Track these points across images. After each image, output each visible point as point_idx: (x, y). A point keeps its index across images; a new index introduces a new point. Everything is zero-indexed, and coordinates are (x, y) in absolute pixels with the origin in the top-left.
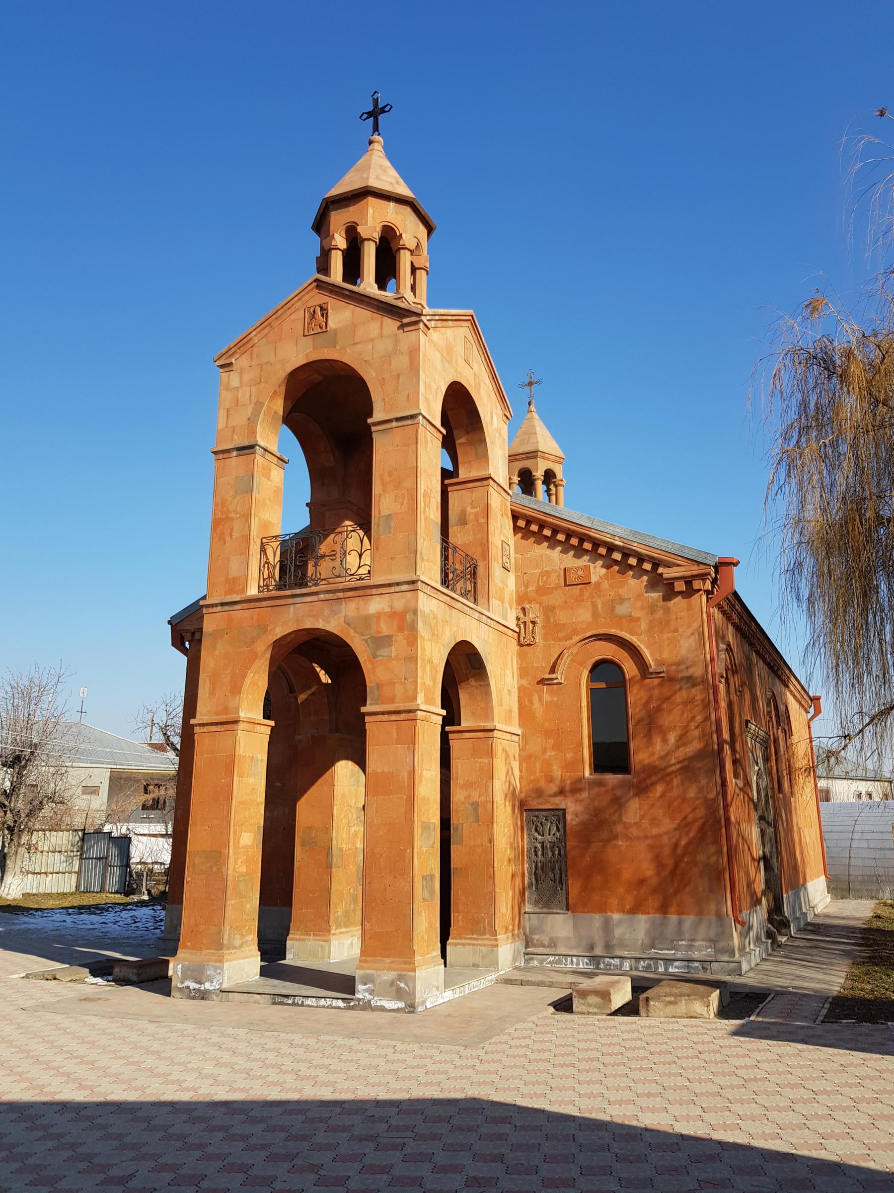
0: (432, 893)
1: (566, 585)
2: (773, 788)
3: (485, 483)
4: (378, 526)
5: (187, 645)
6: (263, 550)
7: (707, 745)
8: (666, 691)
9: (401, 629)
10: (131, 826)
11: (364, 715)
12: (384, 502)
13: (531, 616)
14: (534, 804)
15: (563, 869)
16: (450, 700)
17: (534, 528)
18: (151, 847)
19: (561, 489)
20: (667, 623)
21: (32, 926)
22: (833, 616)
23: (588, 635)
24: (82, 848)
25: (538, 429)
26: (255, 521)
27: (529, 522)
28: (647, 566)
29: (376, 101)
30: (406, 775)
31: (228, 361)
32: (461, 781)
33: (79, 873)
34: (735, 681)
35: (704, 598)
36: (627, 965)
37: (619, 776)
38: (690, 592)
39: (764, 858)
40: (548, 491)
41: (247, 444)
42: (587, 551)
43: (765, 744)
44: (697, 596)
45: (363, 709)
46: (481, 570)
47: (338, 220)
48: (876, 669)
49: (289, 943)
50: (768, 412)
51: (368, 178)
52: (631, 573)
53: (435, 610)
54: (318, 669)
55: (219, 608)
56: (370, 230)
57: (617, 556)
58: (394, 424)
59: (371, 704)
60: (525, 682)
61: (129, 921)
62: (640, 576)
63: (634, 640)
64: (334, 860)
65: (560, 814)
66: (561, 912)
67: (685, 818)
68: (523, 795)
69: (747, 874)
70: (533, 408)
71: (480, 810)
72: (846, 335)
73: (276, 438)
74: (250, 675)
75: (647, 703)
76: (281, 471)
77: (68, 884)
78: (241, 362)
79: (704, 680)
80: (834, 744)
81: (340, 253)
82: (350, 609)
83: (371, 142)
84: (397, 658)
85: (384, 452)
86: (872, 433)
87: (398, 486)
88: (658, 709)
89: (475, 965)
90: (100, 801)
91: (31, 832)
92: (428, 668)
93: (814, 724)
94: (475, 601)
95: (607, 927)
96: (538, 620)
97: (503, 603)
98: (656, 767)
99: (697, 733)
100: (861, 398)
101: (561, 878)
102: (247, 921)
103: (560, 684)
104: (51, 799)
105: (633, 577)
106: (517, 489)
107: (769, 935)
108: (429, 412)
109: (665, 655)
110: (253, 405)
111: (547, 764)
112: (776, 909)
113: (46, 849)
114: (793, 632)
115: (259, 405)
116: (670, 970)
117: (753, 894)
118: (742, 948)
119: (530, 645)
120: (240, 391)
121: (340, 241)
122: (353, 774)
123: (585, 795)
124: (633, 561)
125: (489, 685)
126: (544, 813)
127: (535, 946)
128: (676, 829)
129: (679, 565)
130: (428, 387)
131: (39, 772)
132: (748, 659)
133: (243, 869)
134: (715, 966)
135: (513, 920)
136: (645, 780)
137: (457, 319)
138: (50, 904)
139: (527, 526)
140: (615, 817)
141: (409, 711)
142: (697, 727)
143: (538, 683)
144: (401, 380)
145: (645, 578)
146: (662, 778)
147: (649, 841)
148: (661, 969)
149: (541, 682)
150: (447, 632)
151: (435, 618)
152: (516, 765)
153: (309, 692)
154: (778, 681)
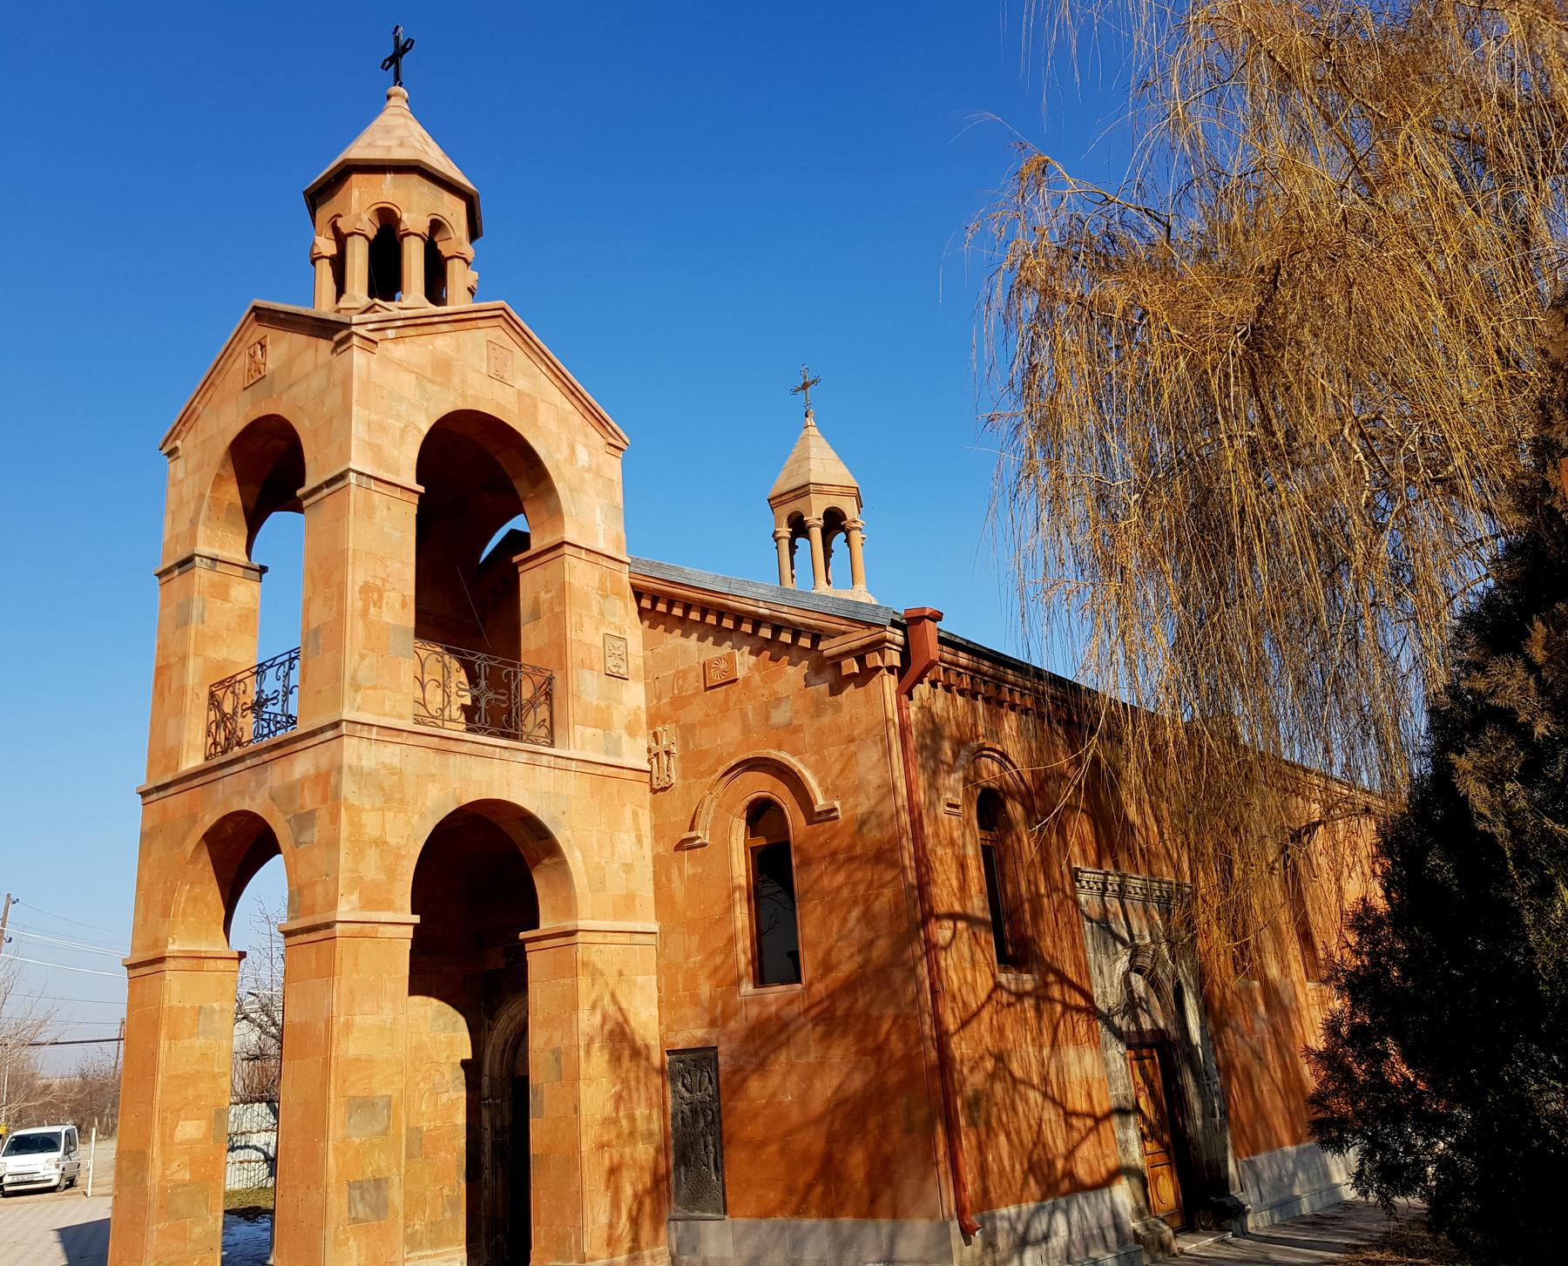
1: (707, 689)
19: (856, 536)
23: (733, 763)
30: (322, 1025)
32: (540, 1017)
38: (865, 675)
46: (558, 685)
58: (326, 491)
66: (715, 1215)
70: (810, 421)
71: (563, 1059)
96: (674, 749)
102: (195, 1252)
103: (704, 845)
108: (379, 466)
119: (664, 789)
129: (844, 633)
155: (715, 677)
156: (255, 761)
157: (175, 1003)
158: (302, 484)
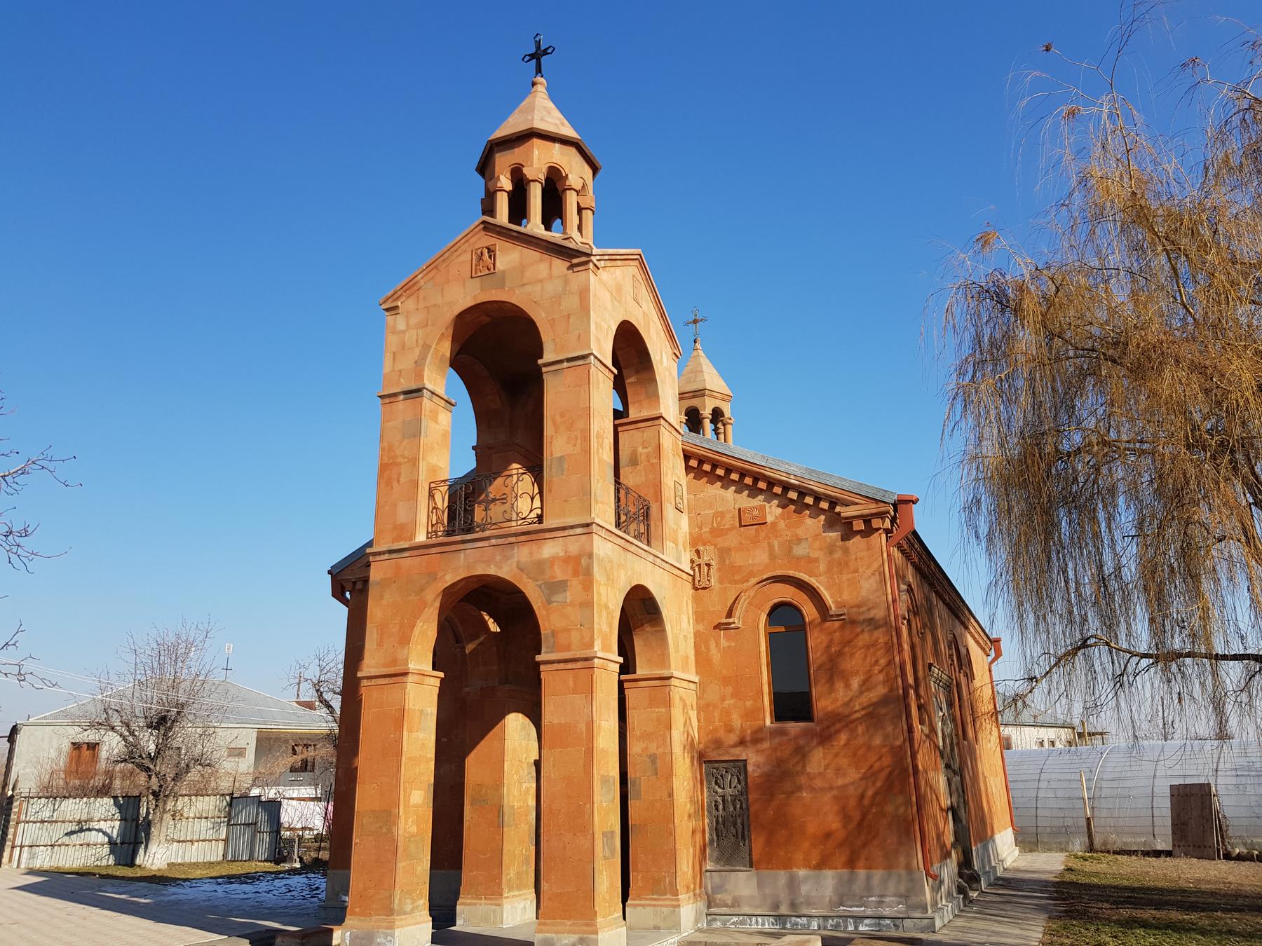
0: (613, 851)
1: (741, 526)
2: (957, 735)
3: (656, 422)
5: (348, 595)
6: (431, 496)
7: (891, 690)
8: (847, 634)
9: (576, 573)
10: (281, 789)
11: (538, 664)
12: (556, 444)
13: (706, 558)
14: (714, 755)
15: (745, 824)
16: (625, 648)
17: (707, 467)
18: (305, 812)
19: (729, 427)
20: (847, 564)
21: (181, 897)
22: (1015, 555)
24: (229, 814)
25: (704, 367)
26: (423, 466)
27: (701, 462)
28: (824, 505)
29: (538, 44)
30: (583, 726)
31: (394, 304)
32: (638, 733)
33: (226, 840)
34: (917, 623)
35: (884, 536)
36: (814, 925)
37: (801, 724)
38: (869, 531)
39: (952, 808)
40: (716, 430)
41: (414, 387)
42: (761, 490)
43: (948, 688)
44: (876, 535)
45: (538, 658)
47: (504, 162)
48: (1060, 606)
49: (459, 908)
50: (943, 347)
51: (532, 120)
52: (807, 512)
53: (610, 553)
54: (487, 617)
55: (387, 556)
56: (536, 170)
57: (793, 495)
58: (566, 365)
60: (701, 627)
61: (283, 889)
62: (818, 515)
63: (813, 581)
64: (506, 818)
65: (740, 766)
67: (871, 767)
68: (702, 746)
69: (937, 825)
70: (698, 345)
71: (658, 761)
72: (1020, 268)
73: (442, 381)
74: (419, 624)
75: (828, 647)
76: (449, 414)
77: (214, 852)
78: (406, 304)
79: (886, 623)
80: (1022, 687)
81: (505, 195)
82: (523, 554)
83: (534, 84)
84: (572, 604)
85: (555, 393)
86: (1048, 367)
87: (570, 427)
88: (840, 653)
89: (657, 928)
90: (246, 764)
91: (176, 797)
92: (604, 613)
93: (994, 666)
94: (649, 544)
95: (793, 884)
97: (677, 545)
98: (839, 714)
99: (881, 677)
100: (1037, 333)
101: (743, 833)
104: (197, 761)
105: (810, 516)
106: (684, 429)
107: (961, 890)
109: (846, 597)
111: (727, 713)
112: (965, 862)
113: (192, 815)
114: (973, 572)
115: (426, 347)
116: (861, 928)
117: (943, 846)
118: (934, 904)
119: (705, 588)
121: (506, 183)
122: (523, 728)
123: (766, 745)
124: (809, 500)
125: (664, 630)
126: (724, 765)
127: (717, 906)
128: (861, 779)
130: (598, 326)
131: (185, 734)
132: (928, 599)
133: (414, 829)
134: (907, 923)
135: (694, 878)
136: (828, 727)
137: (626, 259)
138: (198, 873)
139: (702, 466)
140: (799, 768)
141: (586, 659)
142: (880, 672)
143: (715, 628)
145: (823, 517)
146: (846, 726)
147: (834, 792)
148: (851, 928)
149: (718, 627)
150: (623, 578)
151: (611, 562)
152: (693, 715)
153: (477, 642)
154: (957, 623)
155: (747, 519)
156: (500, 541)
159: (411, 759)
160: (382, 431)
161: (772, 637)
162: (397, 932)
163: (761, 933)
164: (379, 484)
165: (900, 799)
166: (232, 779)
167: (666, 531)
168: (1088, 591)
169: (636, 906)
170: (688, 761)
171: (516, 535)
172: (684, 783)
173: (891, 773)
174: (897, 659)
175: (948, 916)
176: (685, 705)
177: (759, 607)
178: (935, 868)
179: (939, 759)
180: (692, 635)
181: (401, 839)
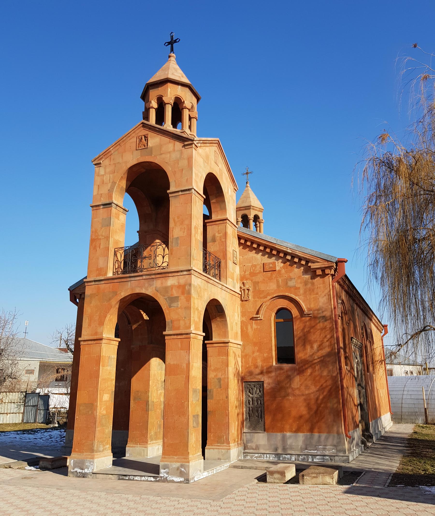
0: (198, 424)
1: (264, 271)
2: (364, 370)
3: (225, 221)
4: (172, 243)
5: (78, 300)
6: (115, 254)
7: (332, 350)
8: (313, 323)
9: (183, 293)
10: (50, 389)
12: (175, 231)
14: (249, 379)
15: (262, 411)
17: (249, 243)
18: (59, 400)
19: (262, 224)
20: (313, 290)
23: (274, 296)
24: (25, 401)
25: (251, 195)
26: (111, 240)
27: (246, 241)
28: (303, 262)
29: (172, 37)
30: (185, 365)
31: (99, 162)
33: (23, 413)
34: (346, 318)
35: (331, 278)
36: (293, 458)
38: (324, 275)
39: (361, 405)
40: (256, 225)
41: (108, 202)
42: (274, 255)
43: (361, 349)
45: (164, 333)
46: (223, 264)
47: (153, 94)
50: (360, 187)
51: (168, 74)
52: (295, 266)
54: (142, 313)
55: (93, 283)
57: (289, 257)
58: (180, 193)
59: (168, 330)
60: (244, 319)
61: (48, 437)
63: (297, 298)
64: (150, 407)
65: (261, 384)
66: (262, 432)
67: (322, 385)
68: (243, 374)
69: (352, 412)
70: (248, 185)
72: (399, 152)
73: (122, 200)
74: (108, 316)
75: (303, 329)
77: (18, 419)
78: (105, 162)
79: (331, 318)
80: (394, 349)
81: (154, 110)
82: (158, 283)
83: (169, 57)
85: (175, 207)
87: (182, 223)
88: (309, 332)
89: (219, 459)
90: (34, 377)
92: (196, 312)
94: (220, 279)
95: (284, 439)
96: (250, 289)
97: (233, 280)
98: (307, 361)
99: (327, 344)
104: (10, 376)
105: (297, 268)
107: (363, 442)
109: (312, 306)
110: (111, 184)
111: (255, 359)
112: (366, 429)
113: (7, 401)
114: (373, 294)
115: (114, 183)
116: (314, 460)
118: (350, 449)
119: (246, 301)
120: (105, 177)
121: (154, 104)
122: (159, 365)
123: (273, 374)
124: (296, 260)
125: (226, 320)
126: (253, 383)
128: (317, 391)
129: (318, 262)
132: (352, 307)
133: (105, 412)
134: (336, 458)
135: (238, 436)
136: (302, 367)
137: (211, 143)
138: (9, 429)
139: (245, 242)
140: (288, 385)
141: (187, 334)
142: (327, 341)
143: (251, 319)
144: (184, 172)
145: (302, 268)
146: (311, 366)
148: (310, 460)
149: (252, 319)
150: (206, 295)
151: (200, 288)
152: (239, 360)
154: (367, 318)
155: (267, 268)
157: (104, 354)
158: (169, 189)
159: (104, 379)
160: (92, 223)
161: (277, 325)
162: (95, 460)
163: (268, 462)
164: (90, 249)
165: (335, 401)
166: (26, 384)
167: (229, 274)
168: (427, 304)
169: (210, 449)
170: (236, 381)
171: (155, 274)
172: (234, 392)
173: (331, 389)
174: (335, 335)
175: (356, 454)
176: (235, 355)
177: (272, 310)
178: (350, 433)
179: (354, 381)
180: (240, 323)
181: (98, 417)
